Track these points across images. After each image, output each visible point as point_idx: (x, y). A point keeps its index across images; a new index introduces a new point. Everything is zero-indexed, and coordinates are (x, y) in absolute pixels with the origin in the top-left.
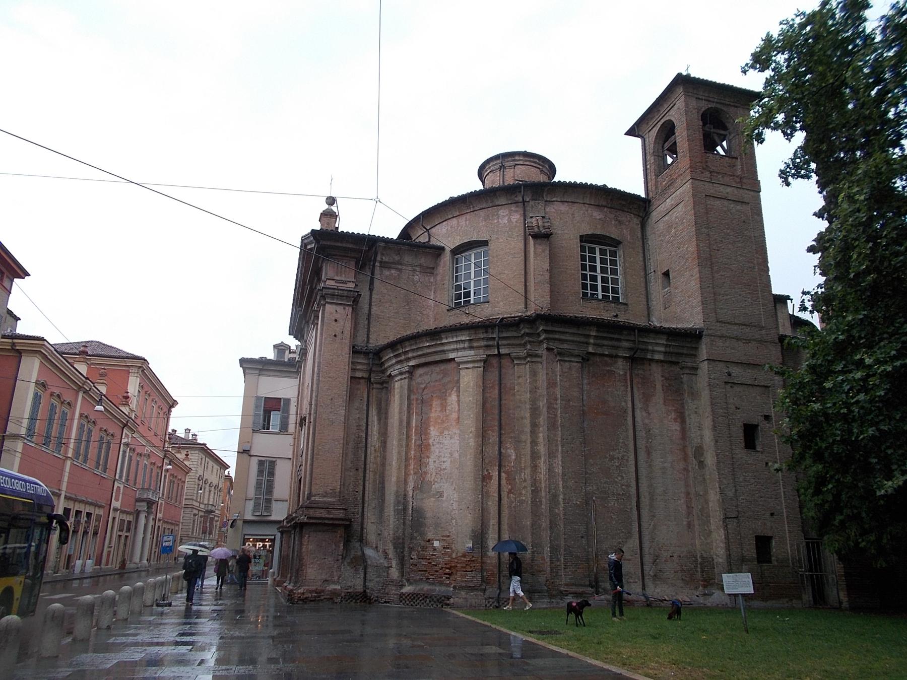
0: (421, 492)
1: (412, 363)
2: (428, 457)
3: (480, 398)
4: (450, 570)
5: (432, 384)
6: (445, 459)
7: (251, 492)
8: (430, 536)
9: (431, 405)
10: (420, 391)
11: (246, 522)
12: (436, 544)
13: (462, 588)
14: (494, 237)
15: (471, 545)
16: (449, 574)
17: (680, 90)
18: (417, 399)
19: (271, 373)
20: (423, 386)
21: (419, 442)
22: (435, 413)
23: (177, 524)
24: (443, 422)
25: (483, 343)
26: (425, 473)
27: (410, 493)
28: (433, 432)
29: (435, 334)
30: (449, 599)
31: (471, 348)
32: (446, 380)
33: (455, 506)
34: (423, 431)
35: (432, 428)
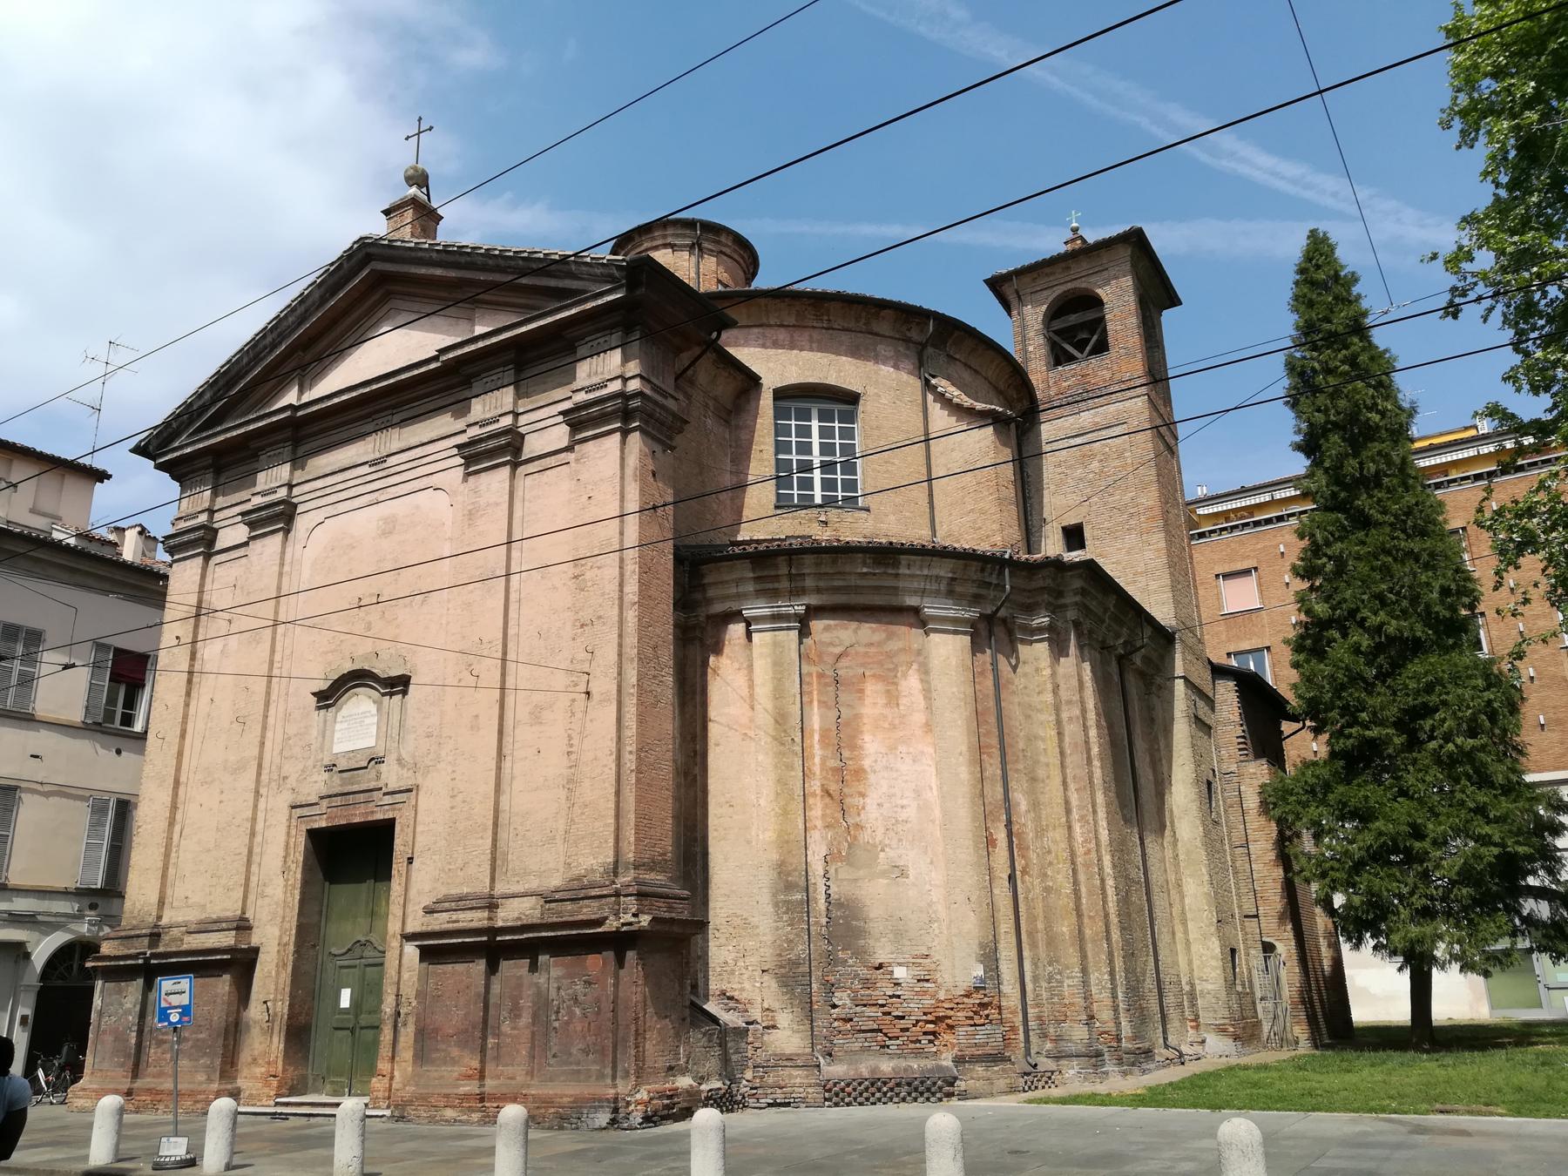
0: (850, 864)
2: (863, 795)
3: (970, 691)
4: (938, 1023)
5: (862, 650)
6: (905, 802)
8: (881, 956)
9: (862, 691)
10: (830, 660)
12: (900, 973)
13: (975, 1059)
14: (871, 390)
15: (980, 972)
16: (933, 1033)
17: (409, 215)
18: (821, 676)
19: (90, 582)
20: (838, 650)
22: (872, 703)
23: (1375, 948)
24: (893, 727)
26: (858, 826)
30: (952, 1084)
33: (937, 895)
34: (843, 737)
35: (867, 737)
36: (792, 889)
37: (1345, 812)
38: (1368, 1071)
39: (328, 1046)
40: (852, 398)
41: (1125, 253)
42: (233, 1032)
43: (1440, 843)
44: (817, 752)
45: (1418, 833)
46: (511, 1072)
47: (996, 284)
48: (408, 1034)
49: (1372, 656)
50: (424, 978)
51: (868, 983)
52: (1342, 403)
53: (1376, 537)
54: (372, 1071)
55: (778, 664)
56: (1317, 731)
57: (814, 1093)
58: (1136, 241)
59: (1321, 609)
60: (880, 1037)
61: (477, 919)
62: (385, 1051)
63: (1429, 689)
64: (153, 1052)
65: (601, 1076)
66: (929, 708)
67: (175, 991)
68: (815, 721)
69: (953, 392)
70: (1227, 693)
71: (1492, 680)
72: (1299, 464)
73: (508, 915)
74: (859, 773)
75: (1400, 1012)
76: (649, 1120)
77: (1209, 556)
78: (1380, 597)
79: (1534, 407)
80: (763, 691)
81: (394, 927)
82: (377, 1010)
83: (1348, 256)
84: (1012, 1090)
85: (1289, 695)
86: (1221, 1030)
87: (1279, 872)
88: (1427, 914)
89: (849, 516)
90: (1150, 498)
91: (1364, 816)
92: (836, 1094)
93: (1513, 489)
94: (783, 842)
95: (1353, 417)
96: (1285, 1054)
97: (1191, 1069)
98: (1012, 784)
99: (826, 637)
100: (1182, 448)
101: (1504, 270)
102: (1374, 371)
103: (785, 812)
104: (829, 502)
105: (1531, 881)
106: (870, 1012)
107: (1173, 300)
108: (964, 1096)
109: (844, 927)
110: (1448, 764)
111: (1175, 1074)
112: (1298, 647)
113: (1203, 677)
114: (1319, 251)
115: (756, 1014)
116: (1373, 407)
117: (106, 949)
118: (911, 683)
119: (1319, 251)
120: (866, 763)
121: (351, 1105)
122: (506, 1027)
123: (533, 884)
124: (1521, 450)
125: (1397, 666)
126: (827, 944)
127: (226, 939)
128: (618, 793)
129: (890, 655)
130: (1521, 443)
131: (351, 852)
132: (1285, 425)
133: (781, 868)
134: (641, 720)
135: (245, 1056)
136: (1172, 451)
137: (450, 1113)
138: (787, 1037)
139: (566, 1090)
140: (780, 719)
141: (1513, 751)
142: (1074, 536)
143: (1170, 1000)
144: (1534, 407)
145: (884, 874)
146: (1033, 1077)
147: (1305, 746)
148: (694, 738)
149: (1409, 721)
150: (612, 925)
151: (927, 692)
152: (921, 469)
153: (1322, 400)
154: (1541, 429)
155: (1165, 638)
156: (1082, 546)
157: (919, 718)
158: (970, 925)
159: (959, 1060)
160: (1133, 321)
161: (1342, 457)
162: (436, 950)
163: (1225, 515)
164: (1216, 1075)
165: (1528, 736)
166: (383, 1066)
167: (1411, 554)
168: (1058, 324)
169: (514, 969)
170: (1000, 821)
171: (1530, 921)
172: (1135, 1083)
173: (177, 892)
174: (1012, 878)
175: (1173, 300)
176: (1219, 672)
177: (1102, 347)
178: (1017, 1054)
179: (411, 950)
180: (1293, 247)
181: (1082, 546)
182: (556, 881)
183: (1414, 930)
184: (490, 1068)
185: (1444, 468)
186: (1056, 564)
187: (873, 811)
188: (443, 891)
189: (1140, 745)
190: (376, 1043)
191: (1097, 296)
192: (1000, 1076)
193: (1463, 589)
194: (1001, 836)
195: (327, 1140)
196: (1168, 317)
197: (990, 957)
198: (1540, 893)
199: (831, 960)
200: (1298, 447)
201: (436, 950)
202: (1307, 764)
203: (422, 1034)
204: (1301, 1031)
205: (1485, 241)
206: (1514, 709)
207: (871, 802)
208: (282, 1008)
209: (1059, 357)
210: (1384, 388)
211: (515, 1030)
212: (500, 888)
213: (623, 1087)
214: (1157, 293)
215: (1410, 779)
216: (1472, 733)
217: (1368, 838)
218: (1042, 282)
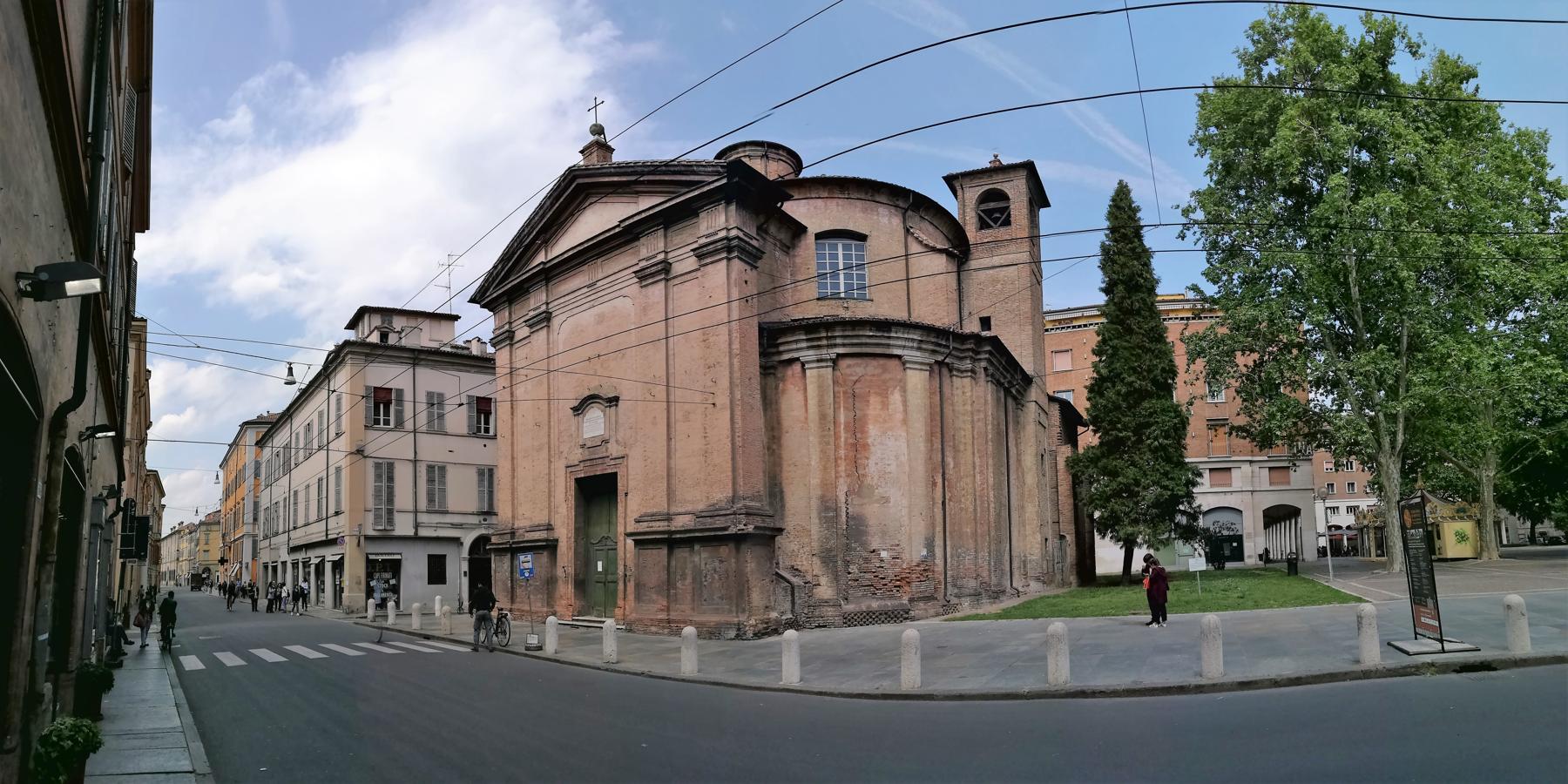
1: (841, 350)
4: (903, 580)
7: (371, 504)
8: (874, 546)
11: (367, 538)
12: (884, 554)
13: (920, 599)
14: (874, 233)
21: (851, 441)
22: (873, 407)
25: (931, 347)
27: (843, 499)
28: (873, 431)
29: (885, 326)
31: (919, 349)
32: (887, 376)
34: (857, 427)
36: (828, 508)
37: (1105, 471)
38: (1104, 597)
39: (598, 592)
40: (862, 238)
41: (1023, 173)
42: (551, 582)
43: (1146, 488)
44: (843, 434)
45: (1137, 483)
46: (683, 609)
47: (950, 180)
48: (631, 586)
49: (1126, 396)
50: (638, 556)
51: (867, 560)
52: (1126, 271)
53: (1135, 339)
54: (615, 605)
55: (821, 388)
56: (1095, 432)
57: (839, 620)
58: (1029, 168)
59: (1104, 372)
60: (872, 589)
61: (660, 526)
62: (620, 595)
63: (1151, 415)
64: (518, 591)
65: (730, 611)
66: (905, 411)
67: (526, 561)
68: (842, 419)
69: (923, 237)
70: (1055, 411)
71: (1176, 410)
72: (1102, 299)
73: (681, 522)
74: (866, 446)
75: (1117, 568)
76: (758, 635)
77: (1053, 340)
78: (1134, 369)
79: (1210, 290)
80: (812, 402)
81: (621, 529)
82: (615, 573)
83: (1138, 196)
84: (937, 615)
85: (1085, 416)
86: (1038, 579)
87: (1071, 501)
88: (1135, 522)
89: (861, 304)
90: (1026, 307)
91: (1113, 474)
92: (850, 620)
93: (1199, 327)
94: (824, 484)
95: (1131, 277)
96: (1066, 590)
97: (1023, 599)
98: (947, 453)
99: (848, 371)
100: (1044, 283)
101: (1209, 222)
102: (1144, 256)
103: (825, 468)
104: (849, 298)
105: (1181, 507)
106: (868, 576)
107: (1046, 204)
108: (913, 619)
109: (855, 529)
110: (1154, 451)
111: (1015, 602)
112: (1091, 389)
113: (1044, 401)
114: (1122, 193)
115: (809, 578)
116: (1141, 275)
117: (494, 540)
118: (896, 397)
119: (1122, 193)
120: (870, 441)
121: (609, 622)
122: (679, 585)
123: (689, 508)
124: (1203, 310)
125: (1137, 403)
126: (847, 537)
127: (542, 535)
128: (733, 459)
129: (884, 382)
130: (1203, 307)
131: (596, 491)
132: (1098, 278)
133: (823, 499)
134: (744, 417)
135: (557, 595)
136: (1039, 283)
137: (654, 629)
138: (825, 591)
139: (713, 619)
140: (823, 417)
141: (1180, 447)
142: (986, 322)
143: (1015, 565)
144: (1210, 290)
145: (877, 501)
146: (948, 607)
147: (1088, 438)
148: (773, 429)
149: (1139, 430)
150: (733, 530)
151: (905, 402)
152: (905, 279)
153: (1116, 267)
154: (1214, 301)
155: (1028, 380)
156: (989, 329)
157: (899, 416)
158: (919, 529)
159: (911, 600)
160: (1025, 211)
161: (1123, 298)
162: (642, 542)
163: (1059, 321)
164: (1035, 601)
165: (1188, 441)
166: (620, 602)
167: (1149, 350)
168: (983, 207)
169: (681, 553)
170: (940, 472)
171: (1178, 525)
172: (995, 608)
173: (521, 510)
174: (944, 503)
175: (1046, 204)
176: (1052, 399)
177: (1007, 223)
178: (940, 596)
179: (630, 542)
180: (1111, 189)
181: (989, 329)
182: (701, 507)
183: (1130, 529)
184: (672, 605)
185: (1168, 312)
186: (975, 337)
187: (872, 467)
188: (644, 511)
189: (1011, 434)
190: (616, 591)
191: (1005, 197)
192: (932, 608)
193: (1173, 372)
194: (939, 481)
195: (599, 640)
196: (1043, 213)
197: (930, 545)
198: (1184, 513)
199: (848, 548)
200: (1102, 290)
201: (642, 542)
202: (1090, 448)
203: (638, 586)
204: (1073, 579)
205: (1203, 207)
206: (1184, 428)
207: (871, 462)
208: (571, 570)
209: (983, 225)
210: (1147, 265)
211: (684, 586)
212: (674, 510)
213: (742, 618)
214: (1038, 198)
215: (1137, 458)
216: (1166, 438)
217: (1114, 485)
218: (976, 182)
